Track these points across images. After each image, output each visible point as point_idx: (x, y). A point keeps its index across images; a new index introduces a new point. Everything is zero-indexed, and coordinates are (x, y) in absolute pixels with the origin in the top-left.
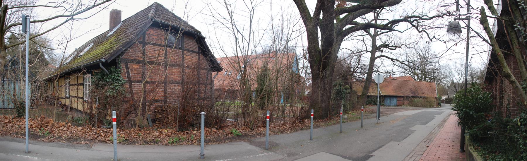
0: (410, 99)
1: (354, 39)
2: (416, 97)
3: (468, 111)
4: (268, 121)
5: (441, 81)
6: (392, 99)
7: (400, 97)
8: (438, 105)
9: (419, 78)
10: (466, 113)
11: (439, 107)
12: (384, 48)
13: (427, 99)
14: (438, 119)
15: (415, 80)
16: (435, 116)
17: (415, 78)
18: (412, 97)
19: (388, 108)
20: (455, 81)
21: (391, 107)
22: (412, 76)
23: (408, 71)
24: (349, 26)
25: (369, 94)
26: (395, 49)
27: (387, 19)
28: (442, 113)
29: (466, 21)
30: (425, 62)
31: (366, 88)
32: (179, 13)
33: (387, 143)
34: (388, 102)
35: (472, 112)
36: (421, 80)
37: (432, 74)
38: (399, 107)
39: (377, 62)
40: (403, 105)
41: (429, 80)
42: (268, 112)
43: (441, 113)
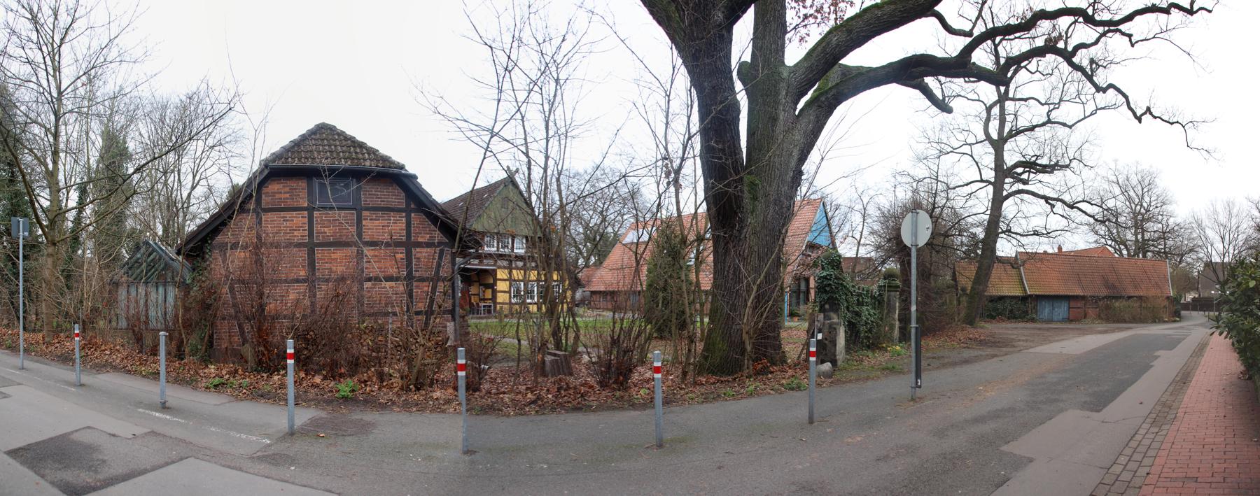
0: (1101, 303)
1: (948, 153)
2: (1116, 298)
4: (813, 361)
6: (1056, 304)
7: (1075, 298)
8: (1173, 317)
11: (1175, 321)
14: (1166, 365)
19: (1040, 329)
21: (1038, 325)
27: (1033, 98)
28: (1179, 341)
34: (1047, 311)
39: (1009, 207)
40: (1085, 317)
43: (1179, 342)
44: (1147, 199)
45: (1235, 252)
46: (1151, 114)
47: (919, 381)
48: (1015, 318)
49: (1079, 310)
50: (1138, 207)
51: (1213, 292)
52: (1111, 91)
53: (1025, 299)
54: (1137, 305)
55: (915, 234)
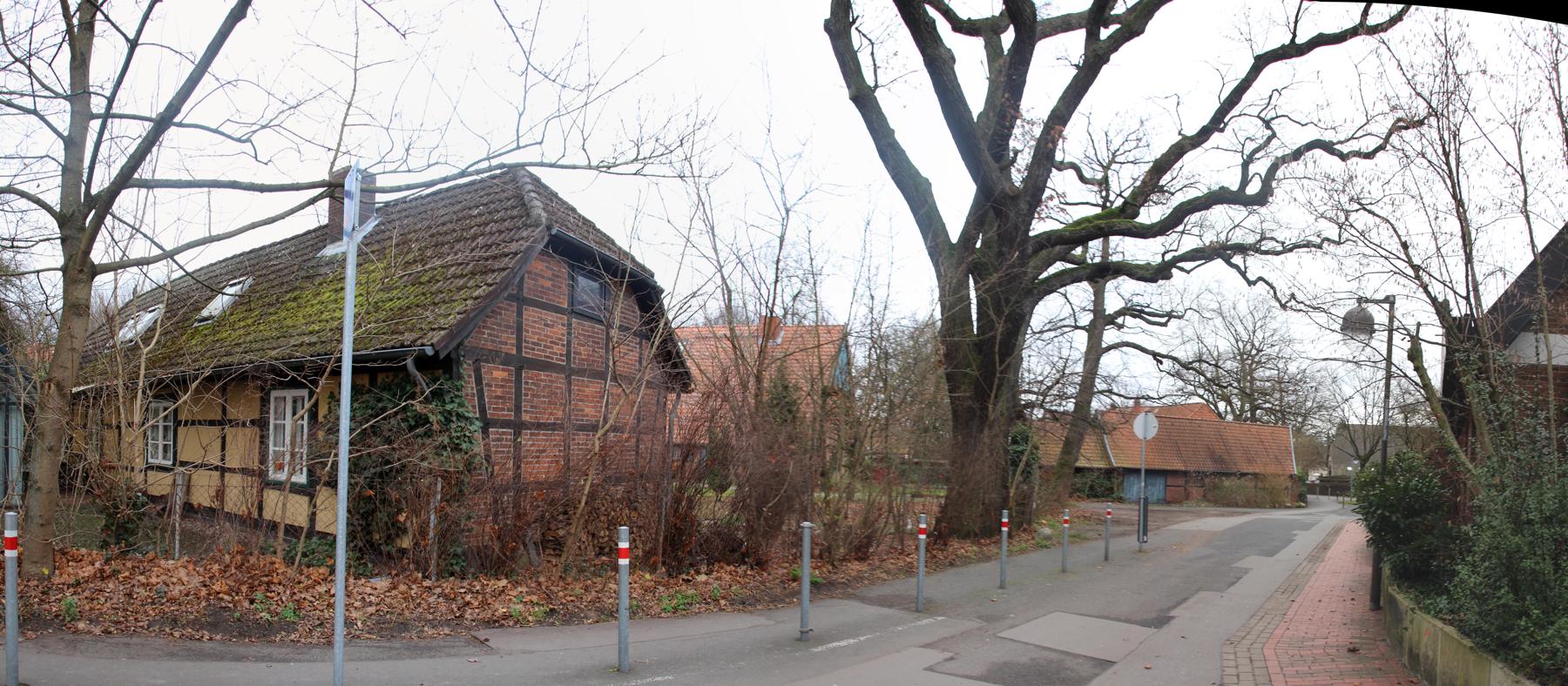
0: (1207, 481)
2: (1228, 475)
3: (1387, 514)
5: (1304, 420)
7: (1175, 473)
9: (1233, 411)
10: (1383, 518)
11: (1300, 507)
14: (1304, 542)
15: (1219, 414)
16: (1295, 532)
17: (1216, 407)
20: (1353, 421)
22: (1207, 401)
24: (1058, 267)
25: (1082, 463)
26: (1165, 325)
29: (1387, 306)
30: (1254, 356)
31: (1071, 446)
32: (622, 242)
33: (1193, 595)
36: (1237, 418)
37: (1277, 395)
39: (1109, 363)
40: (1187, 498)
44: (1259, 334)
46: (1295, 299)
48: (1096, 496)
50: (1248, 347)
51: (1350, 469)
52: (1260, 283)
53: (1110, 472)
54: (1251, 484)
55: (1145, 430)
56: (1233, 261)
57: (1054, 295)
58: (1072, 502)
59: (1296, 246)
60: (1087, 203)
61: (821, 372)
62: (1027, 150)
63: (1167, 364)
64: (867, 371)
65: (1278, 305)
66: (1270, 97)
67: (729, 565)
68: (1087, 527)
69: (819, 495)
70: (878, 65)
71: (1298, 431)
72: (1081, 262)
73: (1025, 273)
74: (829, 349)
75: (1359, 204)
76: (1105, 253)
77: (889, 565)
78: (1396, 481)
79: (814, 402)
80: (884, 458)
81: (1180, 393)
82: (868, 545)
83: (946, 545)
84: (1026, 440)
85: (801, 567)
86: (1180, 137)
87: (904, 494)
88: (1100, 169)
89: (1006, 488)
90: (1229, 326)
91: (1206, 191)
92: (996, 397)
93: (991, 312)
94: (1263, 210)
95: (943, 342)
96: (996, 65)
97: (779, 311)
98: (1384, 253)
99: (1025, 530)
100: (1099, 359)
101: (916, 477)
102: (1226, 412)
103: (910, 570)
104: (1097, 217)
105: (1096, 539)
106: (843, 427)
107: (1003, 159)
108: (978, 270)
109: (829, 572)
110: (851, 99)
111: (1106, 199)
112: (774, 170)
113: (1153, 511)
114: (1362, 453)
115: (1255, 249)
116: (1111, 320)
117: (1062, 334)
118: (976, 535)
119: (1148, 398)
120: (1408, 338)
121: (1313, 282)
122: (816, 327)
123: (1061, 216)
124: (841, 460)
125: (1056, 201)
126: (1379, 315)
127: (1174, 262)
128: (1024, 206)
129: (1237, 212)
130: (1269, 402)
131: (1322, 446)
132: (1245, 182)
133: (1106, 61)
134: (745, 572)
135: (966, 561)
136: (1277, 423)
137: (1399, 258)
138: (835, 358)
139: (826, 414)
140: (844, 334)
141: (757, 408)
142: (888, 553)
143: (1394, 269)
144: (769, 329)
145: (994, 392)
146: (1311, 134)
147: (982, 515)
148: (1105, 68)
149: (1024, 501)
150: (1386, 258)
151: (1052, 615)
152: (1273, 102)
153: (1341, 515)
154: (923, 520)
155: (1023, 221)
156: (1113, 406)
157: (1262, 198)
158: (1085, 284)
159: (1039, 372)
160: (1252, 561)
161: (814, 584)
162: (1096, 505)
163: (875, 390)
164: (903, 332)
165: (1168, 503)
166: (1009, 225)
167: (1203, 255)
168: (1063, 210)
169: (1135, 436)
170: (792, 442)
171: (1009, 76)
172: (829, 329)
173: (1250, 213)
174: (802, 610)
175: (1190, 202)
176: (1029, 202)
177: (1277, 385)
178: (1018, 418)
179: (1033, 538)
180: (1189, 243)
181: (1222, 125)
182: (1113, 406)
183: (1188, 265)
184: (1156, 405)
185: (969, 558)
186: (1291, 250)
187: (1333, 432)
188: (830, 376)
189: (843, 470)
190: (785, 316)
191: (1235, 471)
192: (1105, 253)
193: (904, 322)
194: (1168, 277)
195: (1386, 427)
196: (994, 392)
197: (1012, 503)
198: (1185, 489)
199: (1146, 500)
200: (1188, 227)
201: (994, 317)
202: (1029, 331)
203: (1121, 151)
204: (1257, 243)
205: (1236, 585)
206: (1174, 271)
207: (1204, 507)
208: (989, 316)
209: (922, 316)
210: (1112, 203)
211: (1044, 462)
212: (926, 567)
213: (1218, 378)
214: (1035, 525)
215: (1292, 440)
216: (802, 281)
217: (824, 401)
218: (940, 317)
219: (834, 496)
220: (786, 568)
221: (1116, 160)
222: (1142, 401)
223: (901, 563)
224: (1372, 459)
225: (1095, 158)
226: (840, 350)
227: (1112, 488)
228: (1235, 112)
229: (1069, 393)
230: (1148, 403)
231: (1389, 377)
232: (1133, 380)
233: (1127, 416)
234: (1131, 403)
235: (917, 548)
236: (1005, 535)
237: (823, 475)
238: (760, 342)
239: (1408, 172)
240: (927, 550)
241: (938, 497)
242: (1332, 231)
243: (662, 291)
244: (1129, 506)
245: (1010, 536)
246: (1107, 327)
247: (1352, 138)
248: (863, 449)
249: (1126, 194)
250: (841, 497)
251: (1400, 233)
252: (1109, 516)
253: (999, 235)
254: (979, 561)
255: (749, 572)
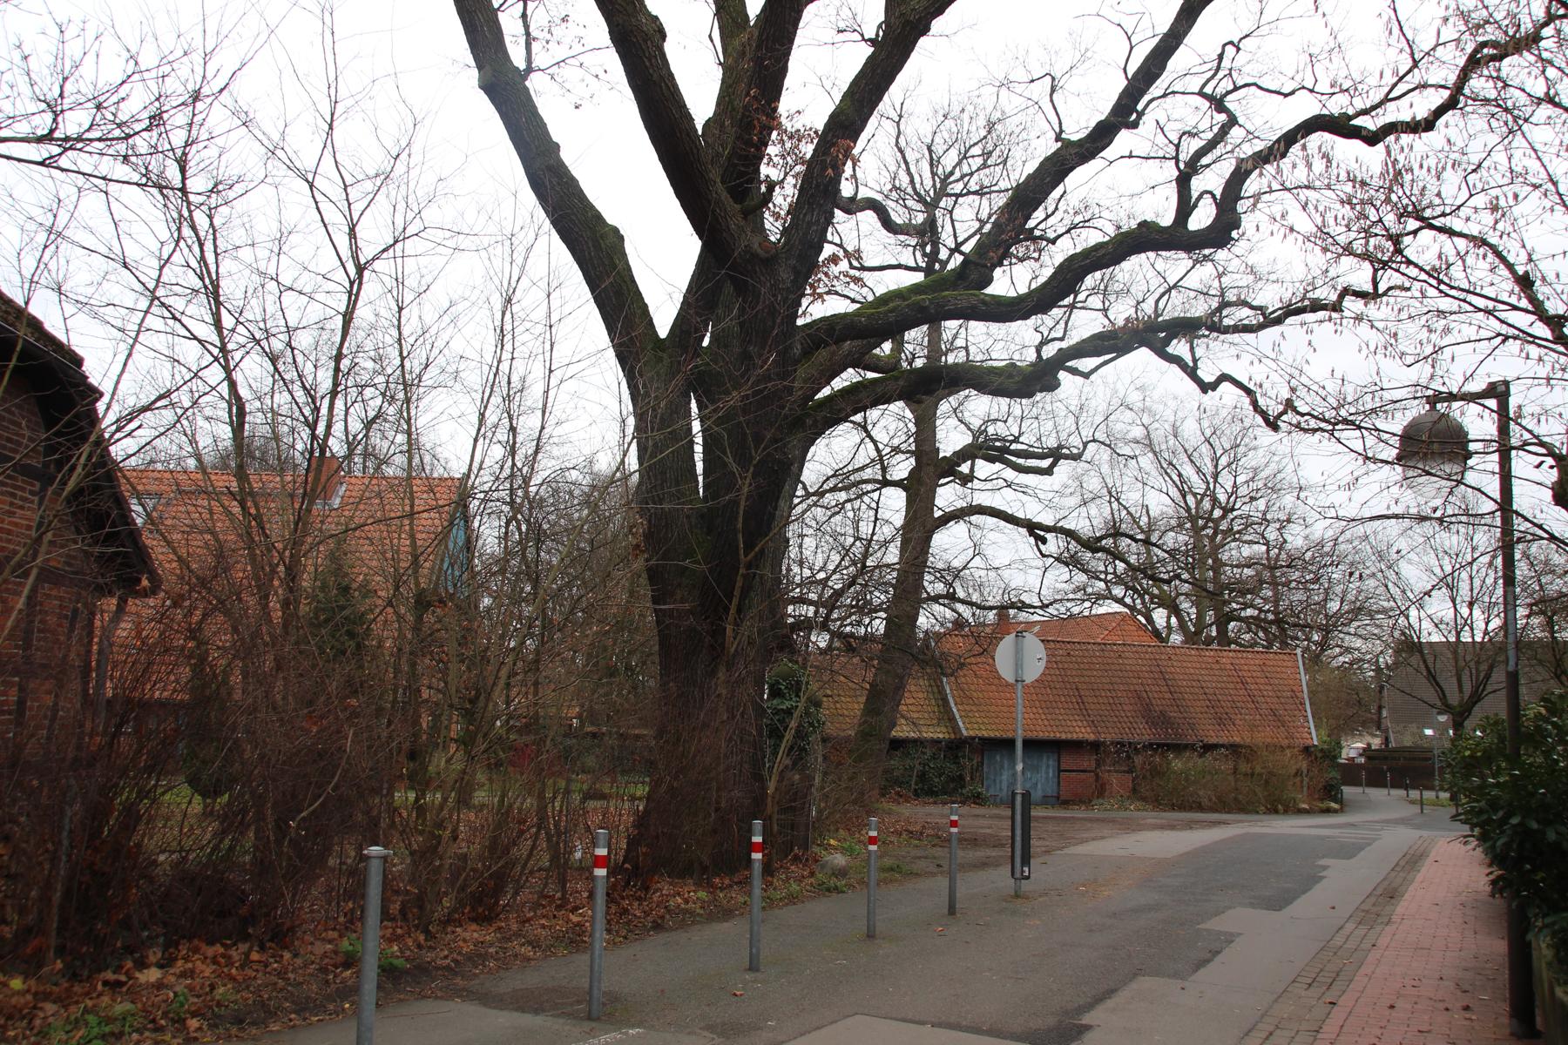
0: (1138, 760)
2: (1179, 748)
3: (1534, 825)
5: (1325, 638)
7: (1076, 746)
8: (1322, 800)
11: (1328, 811)
12: (980, 463)
13: (1248, 761)
15: (1156, 633)
18: (1151, 745)
22: (1132, 608)
23: (1106, 582)
24: (848, 377)
25: (902, 731)
26: (1048, 471)
28: (1361, 848)
29: (1492, 403)
30: (1217, 522)
31: (882, 700)
35: (1557, 833)
36: (1192, 638)
38: (1078, 813)
39: (949, 544)
41: (1250, 630)
42: (601, 837)
44: (1226, 480)
45: (1491, 626)
47: (1026, 869)
48: (931, 793)
49: (1083, 775)
50: (1206, 504)
51: (1429, 732)
53: (956, 747)
54: (1226, 766)
55: (1018, 664)
56: (1170, 350)
57: (844, 427)
58: (886, 805)
59: (1290, 311)
60: (899, 266)
61: (415, 563)
62: (790, 180)
63: (1054, 544)
64: (503, 562)
65: (1259, 420)
66: (1221, 57)
67: (211, 943)
68: (915, 852)
69: (404, 796)
70: (534, 33)
71: (1315, 660)
72: (889, 367)
73: (790, 390)
74: (429, 522)
75: (1422, 219)
76: (935, 349)
77: (537, 930)
78: (1547, 754)
79: (400, 617)
80: (532, 725)
81: (1079, 595)
82: (498, 891)
83: (647, 889)
84: (796, 688)
85: (361, 938)
86: (1059, 144)
87: (567, 792)
88: (919, 206)
89: (760, 779)
90: (1167, 467)
91: (1112, 231)
92: (739, 611)
93: (730, 460)
94: (1221, 255)
95: (642, 512)
96: (736, 42)
97: (337, 446)
98: (1481, 303)
99: (796, 859)
100: (929, 539)
101: (590, 761)
102: (1169, 626)
103: (577, 940)
104: (915, 289)
105: (933, 874)
106: (453, 667)
107: (752, 197)
108: (706, 386)
109: (420, 947)
110: (481, 87)
111: (933, 257)
112: (336, 193)
113: (1037, 819)
114: (1454, 699)
115: (1213, 325)
116: (949, 468)
117: (859, 497)
118: (704, 869)
119: (1023, 606)
120: (1550, 461)
121: (1338, 375)
122: (410, 477)
123: (853, 291)
124: (448, 728)
125: (844, 265)
126: (1478, 423)
127: (1062, 360)
128: (785, 275)
129: (1175, 264)
130: (1252, 606)
131: (1367, 689)
132: (1185, 207)
133: (925, 30)
134: (247, 955)
135: (686, 919)
136: (1270, 646)
137: (1515, 308)
138: (443, 536)
139: (424, 642)
140: (463, 490)
141: (286, 625)
142: (536, 906)
143: (1504, 329)
144: (317, 479)
145: (735, 601)
146: (1304, 108)
147: (715, 831)
148: (923, 42)
149: (794, 802)
150: (1488, 312)
151: (849, 1021)
152: (1226, 63)
153: (1418, 827)
154: (602, 840)
155: (785, 300)
156: (959, 623)
157: (1223, 232)
158: (898, 407)
159: (819, 563)
160: (1234, 917)
161: (389, 973)
162: (932, 809)
163: (517, 599)
164: (571, 493)
165: (1065, 803)
166: (760, 307)
167: (1112, 343)
168: (856, 280)
169: (1000, 678)
170: (355, 693)
171: (758, 61)
172: (432, 485)
173: (1196, 262)
174: (359, 1024)
175: (1087, 253)
176: (794, 268)
177: (1266, 575)
178: (781, 649)
179: (812, 874)
180: (1086, 324)
181: (1134, 116)
182: (959, 623)
183: (1086, 364)
184: (1036, 618)
185: (692, 913)
186: (1279, 321)
187: (1387, 659)
188: (432, 569)
189: (453, 747)
190: (349, 456)
191: (1191, 739)
192: (935, 349)
193: (574, 475)
194: (1052, 386)
195: (1507, 645)
196: (735, 601)
197: (771, 808)
198: (1097, 775)
199: (1026, 796)
200: (1081, 297)
201: (734, 467)
202: (800, 492)
203: (957, 175)
204: (1213, 313)
205: (1211, 966)
206: (1062, 375)
207: (1134, 811)
208: (725, 465)
209: (605, 463)
210: (944, 263)
211: (830, 729)
212: (609, 931)
213: (1152, 565)
214: (816, 849)
215: (1304, 678)
216: (383, 394)
217: (419, 619)
218: (637, 467)
219: (434, 797)
220: (330, 942)
221: (949, 191)
222: (1012, 612)
223: (560, 926)
224: (1478, 712)
225: (910, 190)
226: (451, 524)
227: (961, 778)
228: (1156, 89)
229: (876, 602)
230: (1023, 616)
231: (1507, 546)
232: (992, 574)
233: (983, 640)
234: (991, 615)
235: (591, 895)
236: (757, 868)
237: (412, 756)
238: (297, 506)
239: (1518, 140)
240: (610, 898)
241: (633, 798)
242: (1359, 275)
243: (96, 394)
244: (996, 811)
245: (768, 869)
246: (942, 481)
247: (1386, 100)
248: (491, 706)
249: (967, 248)
250: (445, 799)
251: (1511, 259)
252: (954, 830)
253: (741, 325)
254: (711, 918)
255: (255, 956)
